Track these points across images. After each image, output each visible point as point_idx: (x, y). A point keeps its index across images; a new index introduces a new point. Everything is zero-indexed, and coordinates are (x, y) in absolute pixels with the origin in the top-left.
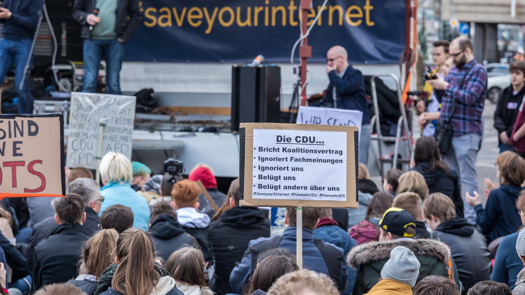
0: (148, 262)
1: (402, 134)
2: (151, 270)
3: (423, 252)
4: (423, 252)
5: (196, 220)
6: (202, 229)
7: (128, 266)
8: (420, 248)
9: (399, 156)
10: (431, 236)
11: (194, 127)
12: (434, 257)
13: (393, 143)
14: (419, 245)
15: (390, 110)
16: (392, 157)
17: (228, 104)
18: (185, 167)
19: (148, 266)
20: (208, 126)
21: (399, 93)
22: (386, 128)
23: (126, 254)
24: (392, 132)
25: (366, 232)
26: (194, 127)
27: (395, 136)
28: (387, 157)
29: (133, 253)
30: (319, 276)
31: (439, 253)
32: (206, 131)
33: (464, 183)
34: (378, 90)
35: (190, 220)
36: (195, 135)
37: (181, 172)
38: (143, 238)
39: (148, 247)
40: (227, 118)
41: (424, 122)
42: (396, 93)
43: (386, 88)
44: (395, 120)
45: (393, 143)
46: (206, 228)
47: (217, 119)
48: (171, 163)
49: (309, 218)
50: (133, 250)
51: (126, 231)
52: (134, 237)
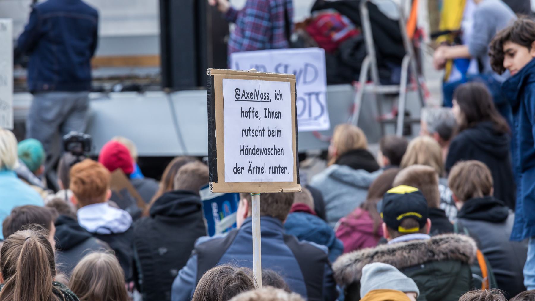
0: (43, 283)
1: (409, 80)
2: (48, 296)
3: (442, 256)
4: (442, 256)
5: (110, 222)
6: (120, 235)
7: (17, 290)
8: (436, 251)
9: (407, 114)
10: (456, 228)
11: (107, 86)
12: (457, 260)
13: (396, 95)
14: (434, 247)
15: (390, 47)
16: (396, 114)
17: (154, 50)
18: (95, 143)
19: (43, 290)
20: (128, 83)
21: (403, 23)
22: (385, 73)
23: (13, 272)
24: (394, 78)
25: (362, 225)
26: (107, 86)
27: (398, 83)
28: (389, 116)
29: (22, 271)
30: (289, 297)
31: (464, 254)
32: (125, 89)
33: (299, 279)
34: (372, 20)
35: (102, 223)
36: (108, 98)
37: (89, 150)
38: (37, 250)
39: (44, 262)
40: (154, 70)
41: (442, 61)
42: (397, 23)
43: (383, 16)
44: (398, 62)
45: (396, 95)
46: (127, 232)
47: (141, 72)
48: (75, 139)
49: (285, 203)
50: (23, 267)
51: (11, 236)
52: (23, 247)
